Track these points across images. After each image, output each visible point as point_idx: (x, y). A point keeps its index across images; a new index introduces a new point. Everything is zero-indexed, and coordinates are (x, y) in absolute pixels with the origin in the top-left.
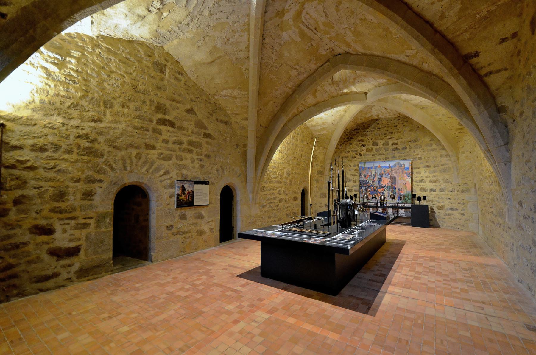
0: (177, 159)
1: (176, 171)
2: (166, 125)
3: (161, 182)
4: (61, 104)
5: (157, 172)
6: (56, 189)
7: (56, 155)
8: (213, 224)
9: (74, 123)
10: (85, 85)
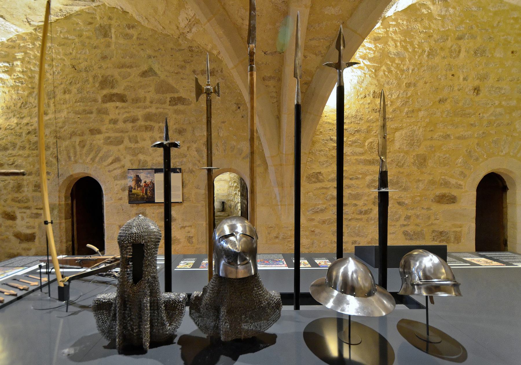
0: (130, 141)
1: (129, 157)
2: (114, 101)
3: (109, 171)
4: (14, 106)
5: (104, 161)
6: (15, 181)
7: (14, 152)
8: (193, 230)
9: (25, 121)
10: (31, 83)
